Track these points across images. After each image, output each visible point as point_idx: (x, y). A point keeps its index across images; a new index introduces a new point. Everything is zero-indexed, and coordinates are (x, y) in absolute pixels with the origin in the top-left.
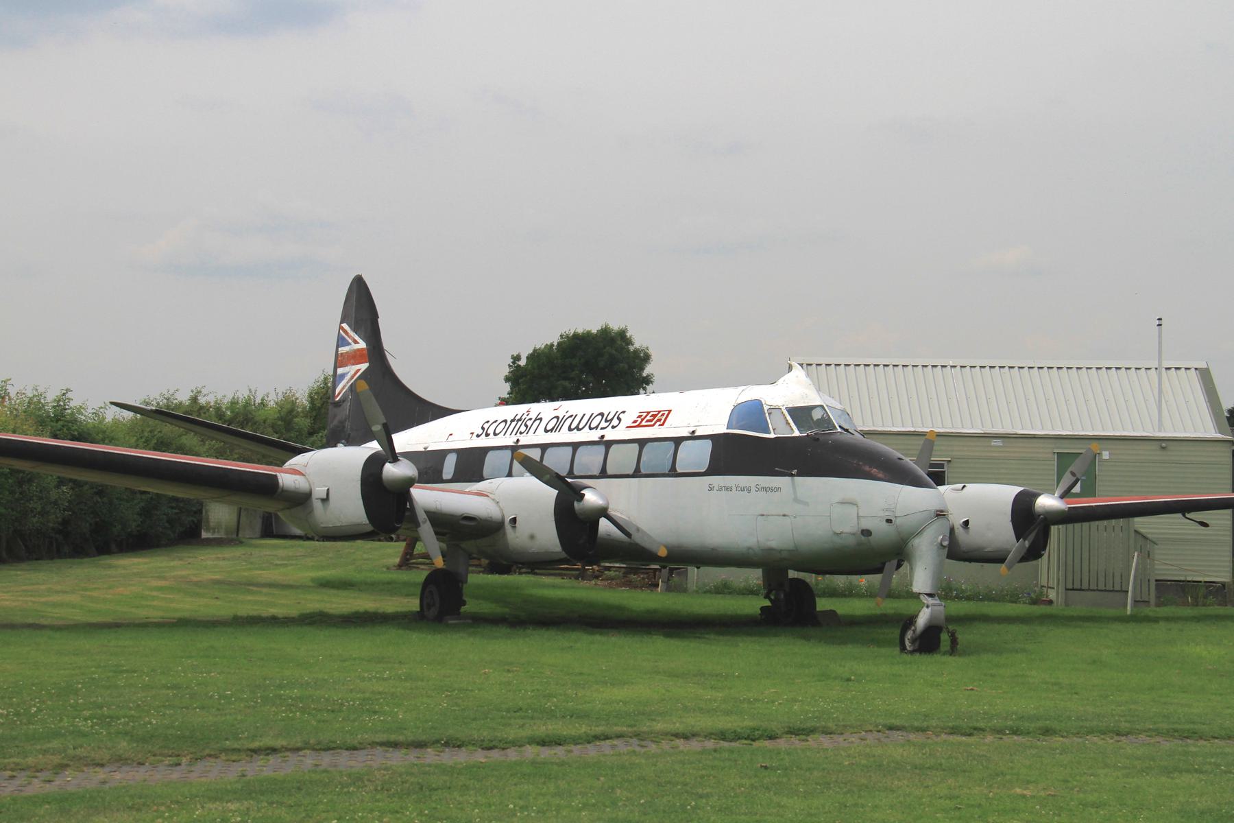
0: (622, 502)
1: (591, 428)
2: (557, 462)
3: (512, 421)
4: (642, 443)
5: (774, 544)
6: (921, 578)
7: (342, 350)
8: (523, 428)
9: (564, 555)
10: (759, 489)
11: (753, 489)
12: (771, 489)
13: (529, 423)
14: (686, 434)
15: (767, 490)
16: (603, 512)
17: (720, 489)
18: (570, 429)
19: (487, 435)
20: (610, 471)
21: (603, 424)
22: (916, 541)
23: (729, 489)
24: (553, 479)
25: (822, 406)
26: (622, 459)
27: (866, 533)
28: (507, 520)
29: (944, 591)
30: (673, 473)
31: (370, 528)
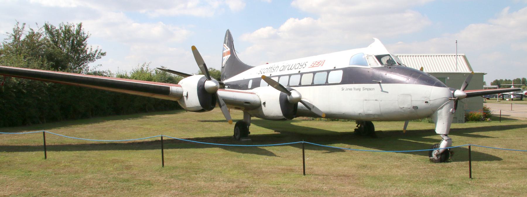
2: (283, 82)
5: (371, 112)
10: (364, 89)
11: (362, 89)
12: (370, 89)
15: (368, 89)
16: (299, 100)
17: (347, 90)
21: (300, 67)
22: (439, 112)
23: (351, 89)
24: (279, 87)
25: (389, 55)
26: (307, 79)
27: (415, 108)
29: (452, 132)
30: (327, 84)
31: (201, 108)
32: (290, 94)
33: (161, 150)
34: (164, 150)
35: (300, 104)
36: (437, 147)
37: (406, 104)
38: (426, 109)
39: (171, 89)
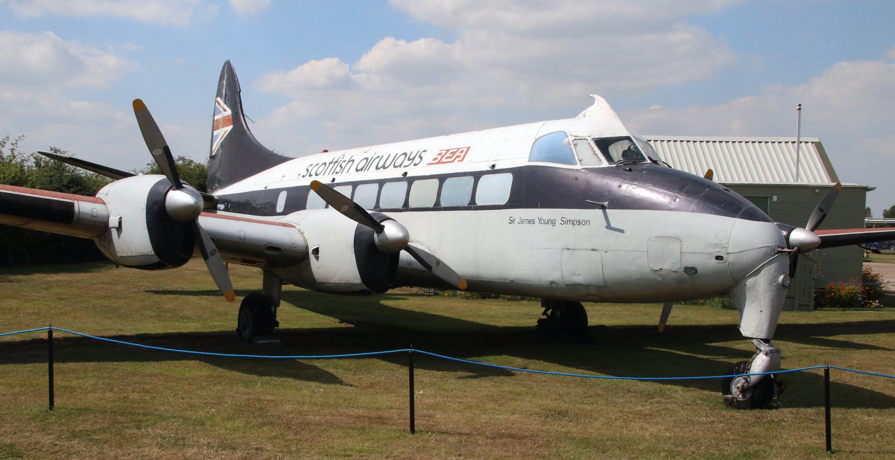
0: (427, 234)
1: (395, 167)
2: (365, 198)
3: (331, 163)
4: (442, 178)
5: (579, 279)
6: (753, 321)
7: (216, 117)
8: (338, 169)
9: (364, 287)
10: (565, 222)
11: (537, 221)
12: (579, 223)
13: (344, 165)
14: (486, 167)
15: (573, 222)
16: (403, 244)
17: (522, 222)
18: (377, 168)
19: (310, 175)
20: (412, 205)
21: (407, 163)
22: (749, 282)
24: (353, 210)
25: (628, 138)
26: (424, 193)
27: (691, 271)
28: (310, 250)
29: (780, 332)
30: (472, 206)
31: (156, 260)
32: (380, 229)
33: (46, 366)
34: (416, 371)
35: (404, 254)
36: (743, 368)
37: (670, 262)
38: (718, 274)
39: (76, 208)
